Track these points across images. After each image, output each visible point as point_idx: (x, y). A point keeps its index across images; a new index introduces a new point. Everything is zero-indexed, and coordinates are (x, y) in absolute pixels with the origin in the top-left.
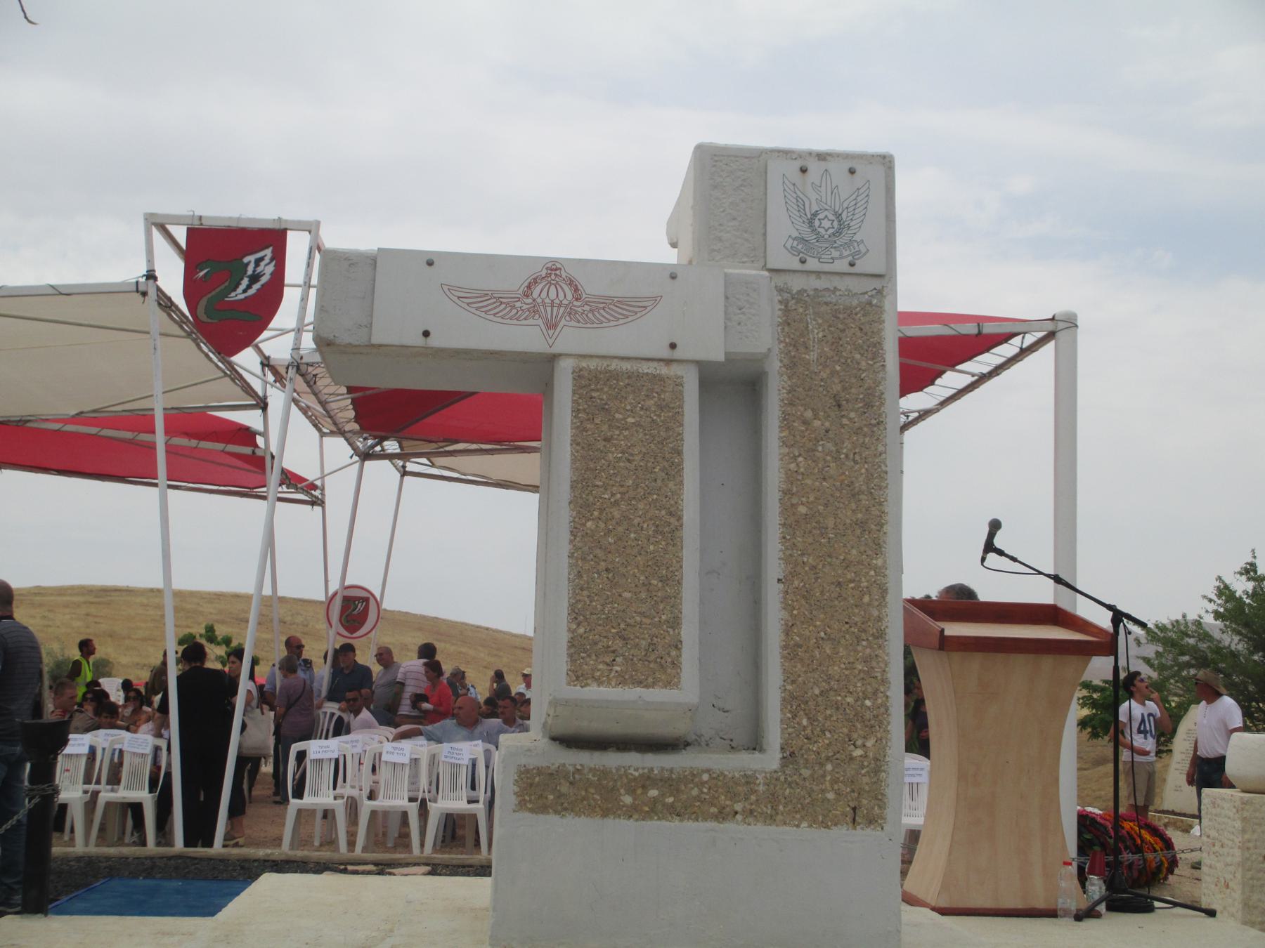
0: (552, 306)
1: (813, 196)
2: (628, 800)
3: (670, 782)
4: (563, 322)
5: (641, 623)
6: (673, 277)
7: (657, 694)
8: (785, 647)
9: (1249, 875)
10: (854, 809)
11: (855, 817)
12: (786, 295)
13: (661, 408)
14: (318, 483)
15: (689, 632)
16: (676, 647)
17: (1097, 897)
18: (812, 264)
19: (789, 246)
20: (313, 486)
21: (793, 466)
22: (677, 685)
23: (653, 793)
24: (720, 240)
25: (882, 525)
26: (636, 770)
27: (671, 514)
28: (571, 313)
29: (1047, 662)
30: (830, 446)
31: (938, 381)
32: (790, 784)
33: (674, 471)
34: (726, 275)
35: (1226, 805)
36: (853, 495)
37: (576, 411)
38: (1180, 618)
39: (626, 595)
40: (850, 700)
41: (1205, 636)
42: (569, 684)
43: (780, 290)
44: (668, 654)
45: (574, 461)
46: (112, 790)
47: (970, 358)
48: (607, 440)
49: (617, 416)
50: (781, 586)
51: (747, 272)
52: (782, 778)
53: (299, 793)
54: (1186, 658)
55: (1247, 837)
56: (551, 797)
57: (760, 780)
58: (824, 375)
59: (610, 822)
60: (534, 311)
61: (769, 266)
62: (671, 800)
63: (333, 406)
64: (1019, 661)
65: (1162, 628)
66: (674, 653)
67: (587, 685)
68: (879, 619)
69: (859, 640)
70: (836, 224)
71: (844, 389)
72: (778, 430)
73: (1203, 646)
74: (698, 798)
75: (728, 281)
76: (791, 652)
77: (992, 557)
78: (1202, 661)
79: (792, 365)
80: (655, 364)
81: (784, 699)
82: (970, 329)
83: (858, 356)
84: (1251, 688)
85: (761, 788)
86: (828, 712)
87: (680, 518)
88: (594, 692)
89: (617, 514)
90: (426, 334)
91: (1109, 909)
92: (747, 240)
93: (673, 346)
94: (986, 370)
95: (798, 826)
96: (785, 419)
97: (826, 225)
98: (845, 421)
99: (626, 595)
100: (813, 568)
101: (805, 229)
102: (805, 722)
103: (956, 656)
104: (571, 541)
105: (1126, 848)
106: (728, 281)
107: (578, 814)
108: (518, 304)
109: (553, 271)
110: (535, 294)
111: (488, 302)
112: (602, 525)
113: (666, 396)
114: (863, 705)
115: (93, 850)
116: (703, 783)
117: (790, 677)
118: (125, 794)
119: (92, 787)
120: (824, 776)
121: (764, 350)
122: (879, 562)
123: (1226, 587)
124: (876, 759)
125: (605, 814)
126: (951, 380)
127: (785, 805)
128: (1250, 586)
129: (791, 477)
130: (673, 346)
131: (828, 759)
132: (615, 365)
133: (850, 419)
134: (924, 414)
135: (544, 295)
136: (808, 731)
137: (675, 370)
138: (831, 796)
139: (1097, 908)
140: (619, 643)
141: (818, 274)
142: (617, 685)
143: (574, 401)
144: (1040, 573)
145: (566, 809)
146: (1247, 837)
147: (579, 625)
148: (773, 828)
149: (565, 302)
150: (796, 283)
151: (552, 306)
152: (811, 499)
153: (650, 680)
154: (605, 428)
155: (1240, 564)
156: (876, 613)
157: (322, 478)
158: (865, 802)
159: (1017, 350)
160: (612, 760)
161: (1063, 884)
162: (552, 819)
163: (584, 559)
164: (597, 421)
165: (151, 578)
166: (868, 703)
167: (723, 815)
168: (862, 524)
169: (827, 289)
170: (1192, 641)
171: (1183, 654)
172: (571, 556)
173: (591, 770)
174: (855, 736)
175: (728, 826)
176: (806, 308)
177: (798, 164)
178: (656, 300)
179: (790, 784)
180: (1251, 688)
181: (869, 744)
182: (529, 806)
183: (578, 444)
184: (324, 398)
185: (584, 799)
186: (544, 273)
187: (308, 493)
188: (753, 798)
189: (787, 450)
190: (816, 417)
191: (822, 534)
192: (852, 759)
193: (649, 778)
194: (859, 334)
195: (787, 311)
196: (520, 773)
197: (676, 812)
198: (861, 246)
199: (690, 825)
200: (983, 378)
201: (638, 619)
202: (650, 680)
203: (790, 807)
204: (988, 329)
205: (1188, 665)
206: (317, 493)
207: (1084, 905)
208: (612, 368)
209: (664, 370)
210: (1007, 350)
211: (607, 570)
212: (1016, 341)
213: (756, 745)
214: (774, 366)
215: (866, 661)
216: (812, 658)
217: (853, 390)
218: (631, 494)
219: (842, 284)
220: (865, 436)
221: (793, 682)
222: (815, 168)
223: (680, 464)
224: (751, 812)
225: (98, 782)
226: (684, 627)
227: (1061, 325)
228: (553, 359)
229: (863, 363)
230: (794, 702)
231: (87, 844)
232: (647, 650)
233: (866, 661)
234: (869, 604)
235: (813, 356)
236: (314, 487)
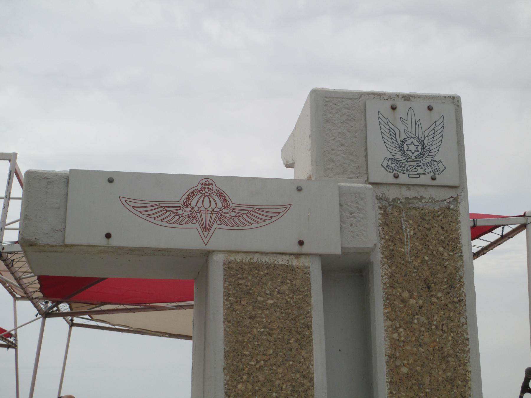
0: (206, 213)
1: (402, 127)
4: (215, 225)
6: (299, 189)
12: (384, 203)
14: (13, 333)
18: (403, 179)
19: (385, 165)
20: (10, 335)
21: (395, 336)
24: (332, 161)
25: (467, 382)
27: (304, 377)
28: (221, 218)
33: (305, 341)
34: (339, 187)
37: (227, 295)
43: (379, 199)
45: (226, 335)
48: (252, 318)
49: (259, 298)
60: (192, 217)
61: (371, 180)
70: (420, 148)
71: (432, 274)
72: (382, 307)
75: (342, 192)
79: (391, 256)
80: (287, 257)
83: (441, 249)
87: (311, 380)
89: (261, 378)
90: (108, 236)
92: (352, 161)
93: (301, 243)
97: (412, 149)
98: (434, 299)
101: (397, 153)
106: (342, 192)
108: (180, 212)
109: (207, 186)
110: (193, 204)
112: (250, 387)
113: (297, 282)
121: (371, 245)
129: (394, 344)
130: (301, 243)
132: (256, 258)
133: (438, 298)
137: (303, 262)
141: (408, 186)
143: (225, 288)
149: (217, 210)
150: (392, 194)
151: (206, 213)
152: (411, 361)
154: (250, 308)
157: (16, 329)
164: (244, 303)
168: (451, 381)
169: (415, 198)
176: (400, 212)
177: (388, 104)
178: (287, 207)
183: (229, 322)
189: (390, 323)
190: (411, 296)
194: (441, 232)
195: (385, 215)
198: (440, 165)
206: (12, 339)
208: (255, 260)
209: (294, 262)
214: (378, 257)
217: (439, 275)
218: (272, 361)
219: (427, 194)
220: (450, 310)
222: (402, 106)
223: (310, 336)
228: (207, 254)
229: (446, 254)
235: (407, 249)
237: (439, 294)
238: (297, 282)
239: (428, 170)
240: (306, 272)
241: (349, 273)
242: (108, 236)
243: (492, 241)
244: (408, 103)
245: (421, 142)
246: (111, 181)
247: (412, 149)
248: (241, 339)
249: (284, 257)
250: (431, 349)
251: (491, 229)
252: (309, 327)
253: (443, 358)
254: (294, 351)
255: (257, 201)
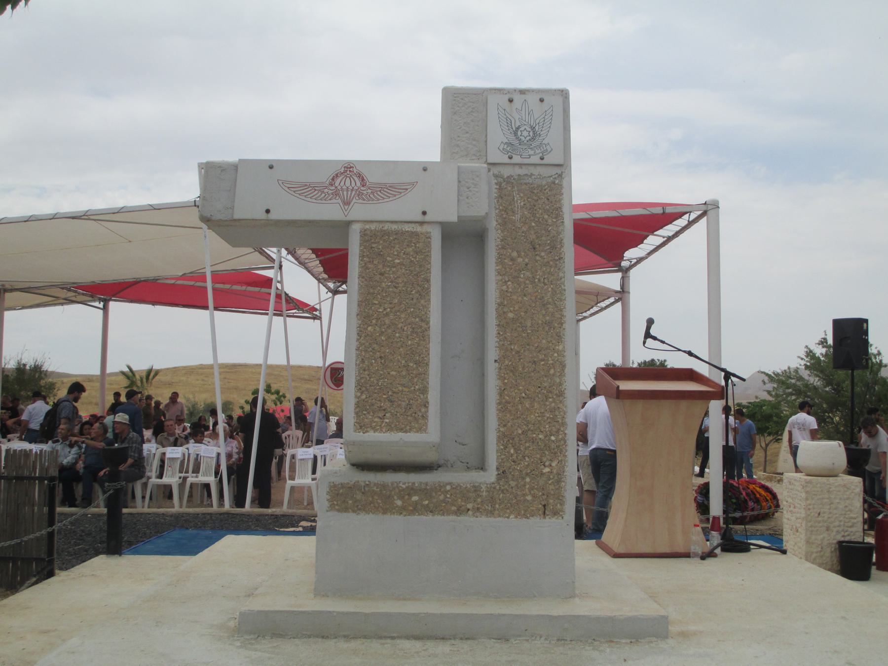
0: (347, 191)
1: (517, 116)
2: (399, 503)
3: (426, 491)
4: (354, 200)
5: (402, 391)
6: (425, 170)
7: (412, 437)
8: (499, 404)
9: (809, 524)
10: (544, 506)
11: (545, 511)
12: (500, 180)
13: (417, 253)
14: (317, 307)
15: (433, 396)
16: (425, 406)
17: (715, 544)
18: (516, 159)
19: (501, 148)
20: (314, 309)
21: (504, 288)
22: (425, 431)
23: (415, 498)
24: (458, 146)
25: (562, 324)
26: (404, 484)
27: (422, 320)
28: (360, 195)
29: (684, 404)
30: (528, 274)
31: (645, 241)
32: (502, 491)
33: (424, 293)
34: (459, 167)
35: (797, 484)
36: (544, 305)
37: (362, 257)
38: (786, 368)
39: (393, 373)
40: (541, 436)
41: (800, 378)
42: (355, 431)
43: (496, 176)
44: (420, 410)
45: (360, 287)
46: (197, 477)
47: (661, 228)
48: (382, 274)
49: (389, 259)
50: (497, 364)
51: (474, 165)
52: (498, 487)
53: (292, 478)
54: (790, 390)
55: (808, 502)
56: (350, 502)
57: (484, 487)
58: (524, 229)
59: (388, 517)
60: (336, 194)
61: (490, 161)
62: (427, 502)
63: (310, 265)
64: (667, 405)
65: (777, 375)
66: (423, 410)
67: (367, 432)
68: (560, 384)
69: (547, 398)
70: (531, 133)
71: (537, 237)
72: (494, 265)
73: (798, 383)
74: (444, 501)
75: (460, 171)
76: (503, 406)
77: (649, 340)
78: (798, 392)
79: (504, 223)
80: (413, 225)
81: (499, 437)
82: (659, 210)
83: (546, 217)
84: (825, 406)
85: (484, 494)
86: (527, 445)
87: (428, 323)
88: (372, 436)
89: (387, 322)
90: (268, 211)
91: (723, 550)
92: (475, 145)
93: (424, 213)
94: (671, 234)
95: (508, 518)
96: (499, 258)
97: (525, 134)
98: (538, 258)
99: (393, 373)
100: (518, 352)
101: (512, 138)
102: (512, 451)
103: (628, 402)
104: (358, 340)
105: (751, 499)
107: (368, 512)
108: (326, 190)
109: (349, 169)
110: (337, 184)
111: (308, 190)
112: (378, 329)
113: (420, 245)
114: (550, 439)
115: (185, 510)
116: (447, 492)
117: (502, 423)
118: (202, 478)
119: (183, 475)
120: (524, 485)
121: (482, 213)
122: (561, 347)
123: (811, 351)
124: (558, 474)
125: (385, 512)
126: (652, 241)
127: (500, 504)
128: (824, 351)
129: (503, 294)
130: (424, 213)
131: (527, 474)
132: (387, 227)
133: (541, 257)
134: (640, 260)
135: (342, 184)
136: (514, 457)
137: (426, 228)
138: (529, 498)
139: (716, 551)
140: (388, 404)
141: (521, 165)
142: (386, 432)
143: (361, 251)
144: (679, 350)
145: (360, 509)
146: (808, 502)
147: (362, 393)
148: (491, 519)
149: (356, 188)
150: (507, 172)
151: (347, 191)
152: (516, 308)
153: (408, 428)
154: (380, 266)
155: (818, 339)
156: (558, 380)
157: (320, 303)
158: (551, 501)
159: (686, 222)
160: (389, 478)
161: (694, 538)
162: (351, 515)
163: (366, 351)
164: (376, 262)
165: (207, 359)
166: (553, 438)
167: (460, 511)
168: (549, 324)
169: (526, 175)
170: (793, 381)
171: (788, 388)
172: (357, 349)
173: (375, 484)
174: (544, 459)
175: (463, 518)
176: (513, 187)
177: (507, 97)
178: (413, 184)
179: (502, 491)
180: (825, 406)
181: (554, 464)
182: (337, 507)
183: (363, 277)
184: (303, 261)
185: (371, 503)
186: (342, 171)
187: (310, 313)
188: (479, 500)
189: (501, 277)
190: (519, 256)
191: (523, 331)
192: (542, 474)
193: (412, 489)
194: (547, 202)
195: (500, 189)
196: (330, 487)
197: (431, 510)
198: (548, 147)
199: (439, 518)
200: (669, 239)
201: (400, 388)
202: (408, 428)
203: (503, 506)
204: (669, 210)
205: (791, 394)
206: (317, 313)
207: (707, 550)
208: (386, 228)
209: (419, 229)
210: (682, 222)
211: (381, 357)
212: (686, 217)
213: (482, 468)
214: (493, 224)
215: (552, 411)
216: (517, 410)
217: (543, 238)
218: (396, 308)
219: (536, 171)
220: (551, 267)
221: (505, 426)
222: (518, 99)
223: (429, 288)
224: (478, 509)
225: (187, 472)
226: (430, 393)
227: (710, 207)
228: (348, 223)
229: (550, 221)
230: (505, 438)
231: (181, 507)
232: (406, 409)
233: (552, 411)
234: (553, 375)
235: (518, 217)
236: (316, 310)
237: (543, 254)
238: (420, 245)
239: (537, 152)
240: (428, 237)
241: (464, 238)
242: (268, 211)
243: (683, 225)
244: (523, 96)
245: (533, 128)
246: (271, 167)
247: (525, 134)
248: (372, 291)
249: (410, 225)
250: (533, 298)
251: (680, 215)
252: (428, 281)
253: (544, 305)
254: (415, 301)
255: (390, 180)
